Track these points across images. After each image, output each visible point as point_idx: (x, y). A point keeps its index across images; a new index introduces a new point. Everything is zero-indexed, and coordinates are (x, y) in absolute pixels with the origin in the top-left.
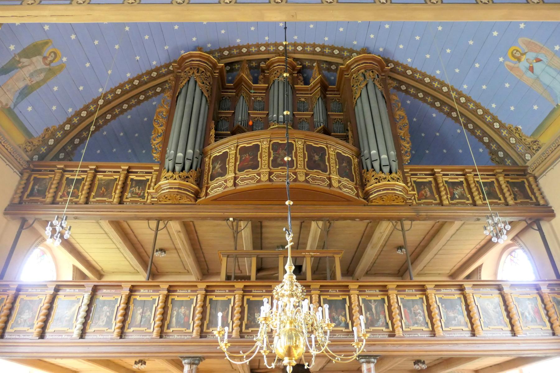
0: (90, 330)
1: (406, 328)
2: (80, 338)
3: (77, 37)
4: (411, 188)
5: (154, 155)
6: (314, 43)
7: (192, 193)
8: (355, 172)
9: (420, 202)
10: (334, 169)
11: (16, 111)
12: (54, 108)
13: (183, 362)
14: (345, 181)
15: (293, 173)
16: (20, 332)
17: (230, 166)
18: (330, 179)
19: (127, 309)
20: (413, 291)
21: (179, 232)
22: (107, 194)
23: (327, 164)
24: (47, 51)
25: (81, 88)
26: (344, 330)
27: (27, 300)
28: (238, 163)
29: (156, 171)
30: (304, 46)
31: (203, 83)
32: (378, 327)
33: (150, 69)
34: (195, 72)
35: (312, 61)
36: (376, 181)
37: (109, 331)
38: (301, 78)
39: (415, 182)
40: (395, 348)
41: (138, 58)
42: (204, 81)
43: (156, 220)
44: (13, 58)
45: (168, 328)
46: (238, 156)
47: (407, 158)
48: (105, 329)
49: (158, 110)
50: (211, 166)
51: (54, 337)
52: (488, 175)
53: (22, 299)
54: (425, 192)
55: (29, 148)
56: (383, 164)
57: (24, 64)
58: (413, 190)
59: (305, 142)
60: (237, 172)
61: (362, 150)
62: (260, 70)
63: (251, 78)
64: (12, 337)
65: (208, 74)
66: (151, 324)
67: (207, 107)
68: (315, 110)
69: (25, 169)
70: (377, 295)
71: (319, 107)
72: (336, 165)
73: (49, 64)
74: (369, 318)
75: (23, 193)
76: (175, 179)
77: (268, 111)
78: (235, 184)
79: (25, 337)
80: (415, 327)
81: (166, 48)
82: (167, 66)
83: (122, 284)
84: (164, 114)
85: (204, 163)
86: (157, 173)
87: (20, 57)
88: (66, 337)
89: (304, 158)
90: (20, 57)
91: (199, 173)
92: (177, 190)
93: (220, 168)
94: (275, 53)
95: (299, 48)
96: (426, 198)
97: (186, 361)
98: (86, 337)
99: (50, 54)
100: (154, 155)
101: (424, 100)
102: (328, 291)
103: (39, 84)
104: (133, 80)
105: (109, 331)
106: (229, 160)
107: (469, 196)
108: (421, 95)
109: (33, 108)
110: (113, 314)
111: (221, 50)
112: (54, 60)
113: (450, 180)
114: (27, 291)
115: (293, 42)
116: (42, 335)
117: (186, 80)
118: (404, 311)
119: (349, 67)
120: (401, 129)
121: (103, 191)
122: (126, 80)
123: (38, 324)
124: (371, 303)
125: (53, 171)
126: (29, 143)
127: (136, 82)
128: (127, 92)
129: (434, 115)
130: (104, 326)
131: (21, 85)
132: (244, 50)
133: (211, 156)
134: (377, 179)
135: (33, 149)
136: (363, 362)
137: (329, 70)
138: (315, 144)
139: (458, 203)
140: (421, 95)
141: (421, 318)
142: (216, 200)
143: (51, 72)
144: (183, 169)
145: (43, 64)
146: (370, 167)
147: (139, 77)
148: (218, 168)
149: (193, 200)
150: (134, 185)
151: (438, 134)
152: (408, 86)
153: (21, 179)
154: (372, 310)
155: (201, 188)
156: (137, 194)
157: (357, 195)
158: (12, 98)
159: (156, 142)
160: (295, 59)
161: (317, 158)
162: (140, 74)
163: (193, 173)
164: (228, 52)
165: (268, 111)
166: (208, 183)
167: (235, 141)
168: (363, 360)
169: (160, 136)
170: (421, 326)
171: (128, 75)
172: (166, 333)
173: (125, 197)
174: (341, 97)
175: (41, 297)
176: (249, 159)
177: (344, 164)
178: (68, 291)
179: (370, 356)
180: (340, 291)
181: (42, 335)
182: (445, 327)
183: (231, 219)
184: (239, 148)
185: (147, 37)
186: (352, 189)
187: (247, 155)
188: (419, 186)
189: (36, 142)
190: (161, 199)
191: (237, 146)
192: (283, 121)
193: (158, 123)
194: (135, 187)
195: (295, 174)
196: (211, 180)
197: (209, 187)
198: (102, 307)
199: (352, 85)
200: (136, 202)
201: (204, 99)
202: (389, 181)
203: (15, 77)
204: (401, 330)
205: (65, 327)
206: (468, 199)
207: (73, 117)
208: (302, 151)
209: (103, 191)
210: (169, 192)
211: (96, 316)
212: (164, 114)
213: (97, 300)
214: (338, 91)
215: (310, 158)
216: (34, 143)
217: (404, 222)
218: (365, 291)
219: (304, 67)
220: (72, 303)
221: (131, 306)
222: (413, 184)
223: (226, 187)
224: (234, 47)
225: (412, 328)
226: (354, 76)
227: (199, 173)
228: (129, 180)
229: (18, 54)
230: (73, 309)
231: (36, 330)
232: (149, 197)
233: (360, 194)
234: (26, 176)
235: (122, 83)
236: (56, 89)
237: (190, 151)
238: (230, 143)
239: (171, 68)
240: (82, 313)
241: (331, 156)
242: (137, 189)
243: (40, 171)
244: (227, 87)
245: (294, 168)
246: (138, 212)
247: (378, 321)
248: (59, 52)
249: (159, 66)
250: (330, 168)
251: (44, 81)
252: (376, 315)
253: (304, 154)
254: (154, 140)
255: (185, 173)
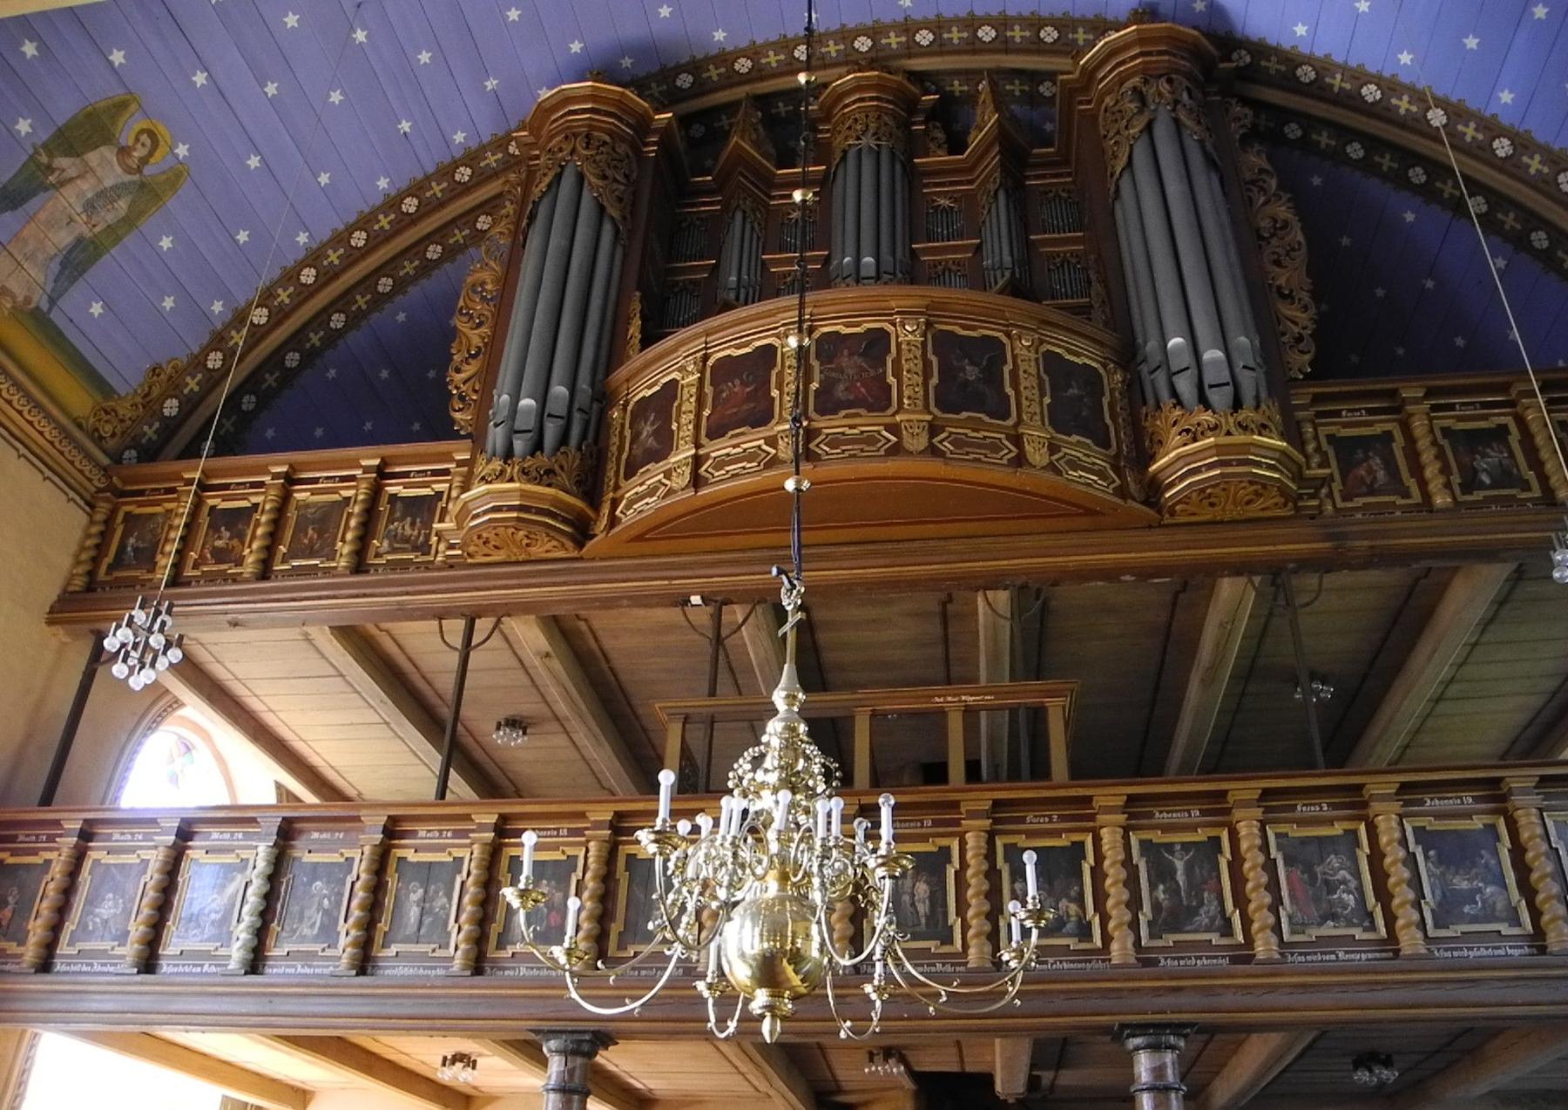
0: (276, 951)
1: (1293, 932)
2: (246, 973)
3: (210, 77)
4: (1316, 460)
5: (457, 416)
6: (971, 13)
7: (565, 521)
8: (1113, 417)
9: (1349, 505)
10: (1036, 408)
11: (55, 316)
12: (168, 303)
13: (545, 1050)
14: (1075, 446)
15: (889, 428)
16: (94, 954)
17: (683, 426)
18: (1017, 440)
19: (377, 889)
20: (1323, 808)
21: (547, 655)
22: (321, 548)
23: (1009, 391)
24: (128, 129)
25: (243, 237)
26: (1073, 943)
27: (108, 866)
28: (706, 413)
29: (460, 463)
30: (938, 26)
31: (604, 177)
32: (1196, 931)
33: (447, 160)
34: (580, 144)
35: (970, 75)
36: (1185, 437)
37: (329, 953)
38: (940, 135)
39: (1331, 438)
40: (1249, 1000)
41: (405, 126)
42: (609, 173)
43: (463, 615)
44: (31, 158)
45: (501, 945)
46: (708, 389)
47: (1301, 361)
48: (317, 947)
49: (469, 280)
50: (628, 433)
51: (181, 969)
52: (1485, 405)
53: (97, 862)
54: (1370, 471)
55: (108, 428)
56: (1207, 380)
57: (66, 175)
58: (1324, 464)
59: (929, 324)
60: (704, 440)
61: (1140, 341)
62: (787, 122)
63: (772, 151)
64: (73, 968)
65: (622, 149)
66: (449, 934)
67: (619, 251)
68: (986, 233)
69: (100, 490)
70: (1193, 828)
71: (998, 220)
72: (1042, 395)
73: (139, 170)
74: (1165, 904)
75: (96, 561)
76: (511, 480)
77: (829, 248)
78: (697, 481)
79: (105, 969)
80: (1329, 929)
81: (491, 84)
82: (501, 143)
83: (363, 812)
84: (489, 287)
85: (609, 426)
86: (465, 469)
87: (51, 155)
88: (213, 969)
89: (927, 375)
90: (51, 155)
91: (585, 456)
92: (515, 515)
93: (655, 433)
94: (846, 63)
95: (924, 38)
96: (1372, 492)
97: (553, 1044)
98: (268, 970)
99: (137, 140)
100: (457, 416)
101: (1366, 166)
102: (1022, 820)
103: (115, 233)
104: (400, 198)
105: (329, 953)
106: (680, 405)
107: (1531, 475)
108: (1355, 151)
109: (106, 305)
110: (339, 904)
111: (667, 74)
112: (151, 154)
113: (1461, 426)
114: (109, 838)
115: (900, 19)
116: (148, 963)
117: (551, 175)
118: (1288, 878)
119: (1089, 74)
120: (1278, 263)
121: (311, 540)
122: (379, 201)
123: (137, 930)
124: (1172, 853)
125: (173, 490)
126: (107, 413)
127: (410, 205)
128: (388, 237)
129: (1410, 217)
130: (316, 939)
131: (64, 238)
132: (743, 65)
133: (627, 403)
134: (1188, 431)
135: (118, 430)
136: (1137, 1049)
137: (1033, 99)
138: (964, 327)
139: (1488, 501)
140: (1355, 151)
141: (1350, 899)
142: (640, 538)
143: (148, 193)
144: (537, 446)
145: (119, 170)
146: (1164, 393)
147: (416, 189)
148: (648, 436)
149: (569, 544)
150: (398, 514)
151: (1430, 284)
152: (1310, 122)
153: (92, 522)
154: (1173, 878)
155: (596, 507)
156: (407, 540)
157: (1122, 492)
158: (41, 279)
159: (461, 377)
160: (913, 76)
161: (971, 373)
162: (420, 176)
163: (572, 457)
164: (690, 79)
165: (829, 248)
166: (617, 487)
167: (699, 344)
168: (1138, 1041)
169: (474, 357)
170: (1350, 924)
171: (383, 183)
172: (495, 960)
173: (372, 552)
174: (1074, 182)
175: (145, 855)
176: (741, 391)
177: (1073, 391)
178: (216, 835)
179: (1160, 1027)
180: (1062, 818)
181: (148, 963)
182: (1437, 926)
183: (696, 599)
184: (710, 363)
185: (425, 57)
186: (1102, 474)
187: (737, 382)
188: (1348, 451)
189: (125, 411)
190: (472, 549)
191: (706, 358)
192: (873, 274)
193: (471, 317)
194: (402, 519)
195: (894, 429)
196: (628, 476)
197: (622, 497)
198: (310, 883)
199: (1103, 132)
200: (404, 565)
201: (607, 229)
202: (1229, 433)
203: (43, 216)
204: (1419, 935)
205: (208, 940)
206: (1526, 486)
207: (229, 326)
208: (919, 353)
209: (311, 540)
210: (518, 519)
211: (295, 909)
212: (489, 287)
213: (296, 864)
214: (1066, 162)
215: (992, 376)
216: (121, 412)
217: (1295, 581)
218: (1150, 815)
219: (947, 100)
220: (228, 871)
221: (392, 881)
222: (1325, 446)
223: (670, 492)
224: (709, 59)
225: (1314, 933)
226: (1109, 101)
227: (585, 456)
228: (384, 499)
229: (45, 146)
230: (231, 889)
231: (130, 950)
232: (442, 547)
233: (1133, 487)
234: (103, 509)
235: (367, 210)
236: (166, 243)
237: (559, 390)
238: (682, 352)
239: (513, 149)
240: (253, 899)
241: (1022, 366)
242: (407, 527)
243: (141, 493)
244: (680, 180)
245: (890, 411)
246: (407, 593)
247: (1193, 912)
248: (162, 130)
249: (474, 145)
250: (1019, 405)
251: (129, 222)
252: (1189, 895)
253: (927, 365)
254: (458, 371)
255: (543, 460)
